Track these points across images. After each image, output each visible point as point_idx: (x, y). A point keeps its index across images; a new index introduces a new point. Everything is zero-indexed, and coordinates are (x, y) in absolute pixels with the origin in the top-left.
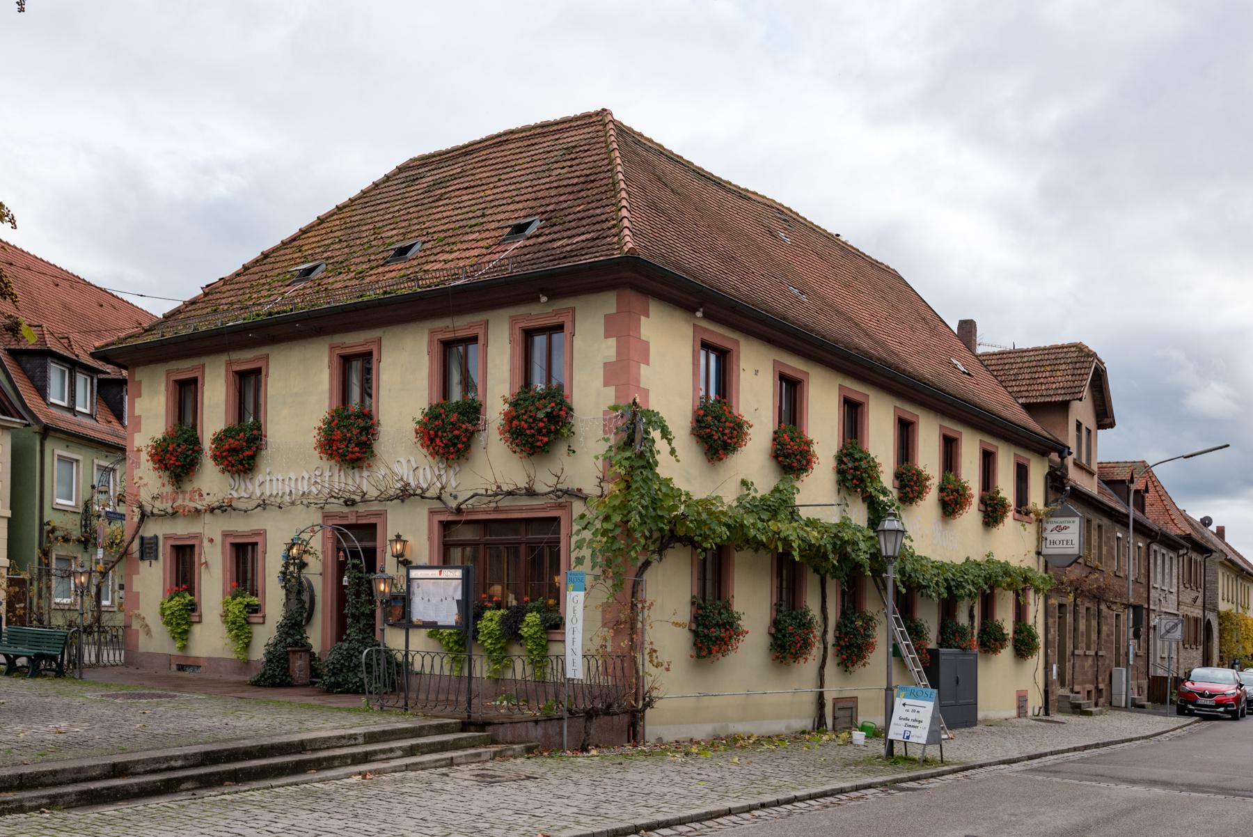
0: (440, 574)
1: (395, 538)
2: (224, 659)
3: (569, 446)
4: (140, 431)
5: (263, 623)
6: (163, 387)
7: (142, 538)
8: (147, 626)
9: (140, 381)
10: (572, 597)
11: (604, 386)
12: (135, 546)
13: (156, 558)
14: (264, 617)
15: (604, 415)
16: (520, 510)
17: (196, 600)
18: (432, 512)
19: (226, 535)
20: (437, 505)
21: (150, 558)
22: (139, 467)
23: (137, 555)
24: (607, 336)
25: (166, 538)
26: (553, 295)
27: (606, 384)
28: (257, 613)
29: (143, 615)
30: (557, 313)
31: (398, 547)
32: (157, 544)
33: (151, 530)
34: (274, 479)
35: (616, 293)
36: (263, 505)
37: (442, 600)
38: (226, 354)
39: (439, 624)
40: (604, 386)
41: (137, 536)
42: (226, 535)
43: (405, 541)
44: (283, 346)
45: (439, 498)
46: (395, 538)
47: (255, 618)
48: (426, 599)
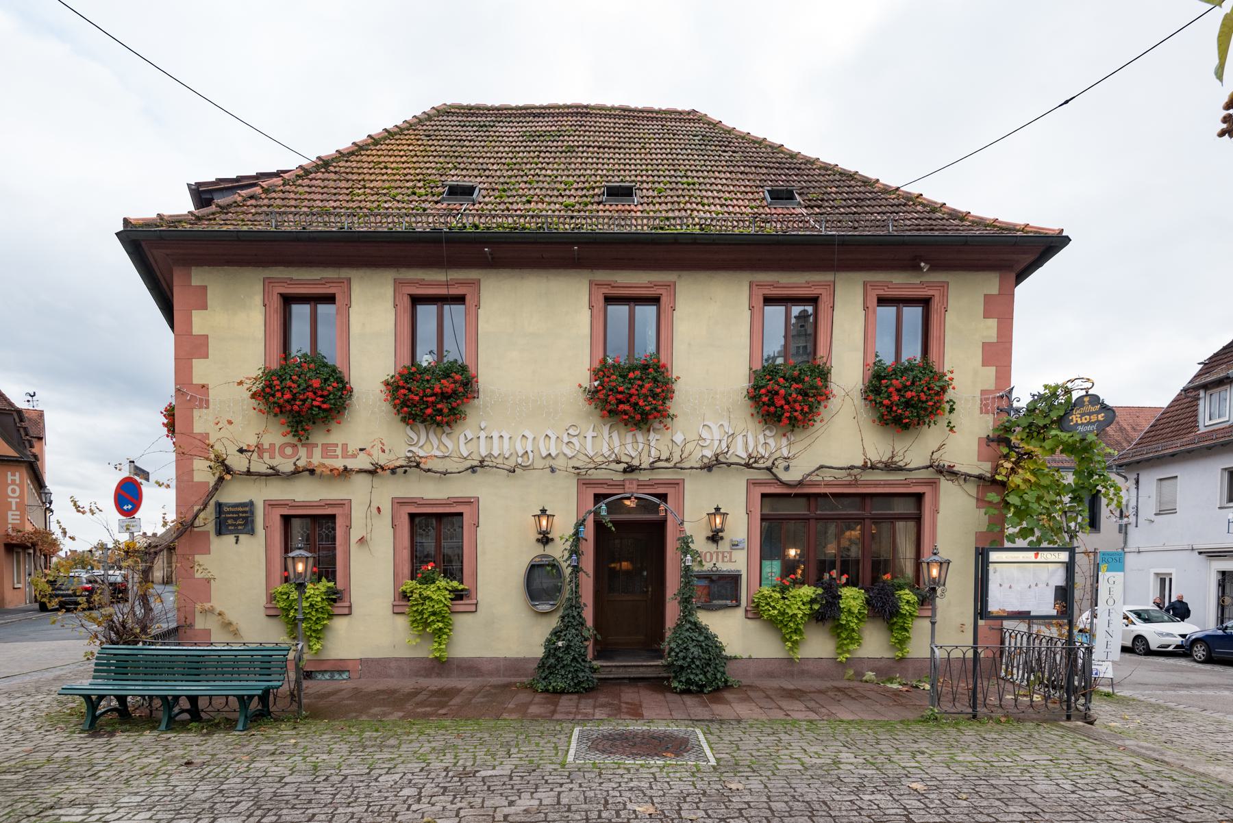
0: (1036, 557)
1: (714, 511)
2: (397, 659)
3: (950, 422)
4: (206, 356)
5: (350, 614)
6: (258, 300)
7: (219, 506)
8: (230, 624)
9: (205, 288)
10: (1106, 578)
11: (983, 365)
12: (209, 515)
13: (252, 532)
14: (350, 607)
15: (981, 395)
16: (876, 485)
17: (340, 586)
18: (752, 484)
19: (399, 503)
20: (764, 476)
21: (236, 532)
22: (207, 408)
23: (211, 527)
24: (987, 315)
25: (270, 505)
26: (935, 267)
27: (985, 363)
28: (462, 599)
29: (218, 609)
30: (930, 285)
31: (718, 520)
32: (252, 513)
33: (234, 494)
34: (495, 435)
35: (998, 275)
36: (481, 466)
37: (1030, 587)
38: (444, 270)
39: (1032, 614)
40: (983, 365)
41: (212, 502)
42: (399, 503)
43: (724, 514)
44: (505, 273)
45: (769, 469)
46: (714, 511)
47: (460, 606)
48: (1006, 586)
